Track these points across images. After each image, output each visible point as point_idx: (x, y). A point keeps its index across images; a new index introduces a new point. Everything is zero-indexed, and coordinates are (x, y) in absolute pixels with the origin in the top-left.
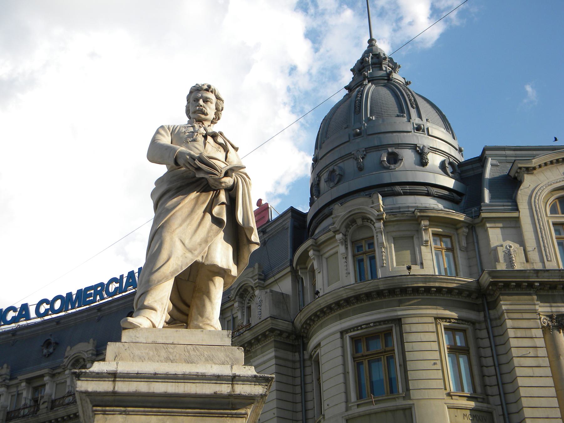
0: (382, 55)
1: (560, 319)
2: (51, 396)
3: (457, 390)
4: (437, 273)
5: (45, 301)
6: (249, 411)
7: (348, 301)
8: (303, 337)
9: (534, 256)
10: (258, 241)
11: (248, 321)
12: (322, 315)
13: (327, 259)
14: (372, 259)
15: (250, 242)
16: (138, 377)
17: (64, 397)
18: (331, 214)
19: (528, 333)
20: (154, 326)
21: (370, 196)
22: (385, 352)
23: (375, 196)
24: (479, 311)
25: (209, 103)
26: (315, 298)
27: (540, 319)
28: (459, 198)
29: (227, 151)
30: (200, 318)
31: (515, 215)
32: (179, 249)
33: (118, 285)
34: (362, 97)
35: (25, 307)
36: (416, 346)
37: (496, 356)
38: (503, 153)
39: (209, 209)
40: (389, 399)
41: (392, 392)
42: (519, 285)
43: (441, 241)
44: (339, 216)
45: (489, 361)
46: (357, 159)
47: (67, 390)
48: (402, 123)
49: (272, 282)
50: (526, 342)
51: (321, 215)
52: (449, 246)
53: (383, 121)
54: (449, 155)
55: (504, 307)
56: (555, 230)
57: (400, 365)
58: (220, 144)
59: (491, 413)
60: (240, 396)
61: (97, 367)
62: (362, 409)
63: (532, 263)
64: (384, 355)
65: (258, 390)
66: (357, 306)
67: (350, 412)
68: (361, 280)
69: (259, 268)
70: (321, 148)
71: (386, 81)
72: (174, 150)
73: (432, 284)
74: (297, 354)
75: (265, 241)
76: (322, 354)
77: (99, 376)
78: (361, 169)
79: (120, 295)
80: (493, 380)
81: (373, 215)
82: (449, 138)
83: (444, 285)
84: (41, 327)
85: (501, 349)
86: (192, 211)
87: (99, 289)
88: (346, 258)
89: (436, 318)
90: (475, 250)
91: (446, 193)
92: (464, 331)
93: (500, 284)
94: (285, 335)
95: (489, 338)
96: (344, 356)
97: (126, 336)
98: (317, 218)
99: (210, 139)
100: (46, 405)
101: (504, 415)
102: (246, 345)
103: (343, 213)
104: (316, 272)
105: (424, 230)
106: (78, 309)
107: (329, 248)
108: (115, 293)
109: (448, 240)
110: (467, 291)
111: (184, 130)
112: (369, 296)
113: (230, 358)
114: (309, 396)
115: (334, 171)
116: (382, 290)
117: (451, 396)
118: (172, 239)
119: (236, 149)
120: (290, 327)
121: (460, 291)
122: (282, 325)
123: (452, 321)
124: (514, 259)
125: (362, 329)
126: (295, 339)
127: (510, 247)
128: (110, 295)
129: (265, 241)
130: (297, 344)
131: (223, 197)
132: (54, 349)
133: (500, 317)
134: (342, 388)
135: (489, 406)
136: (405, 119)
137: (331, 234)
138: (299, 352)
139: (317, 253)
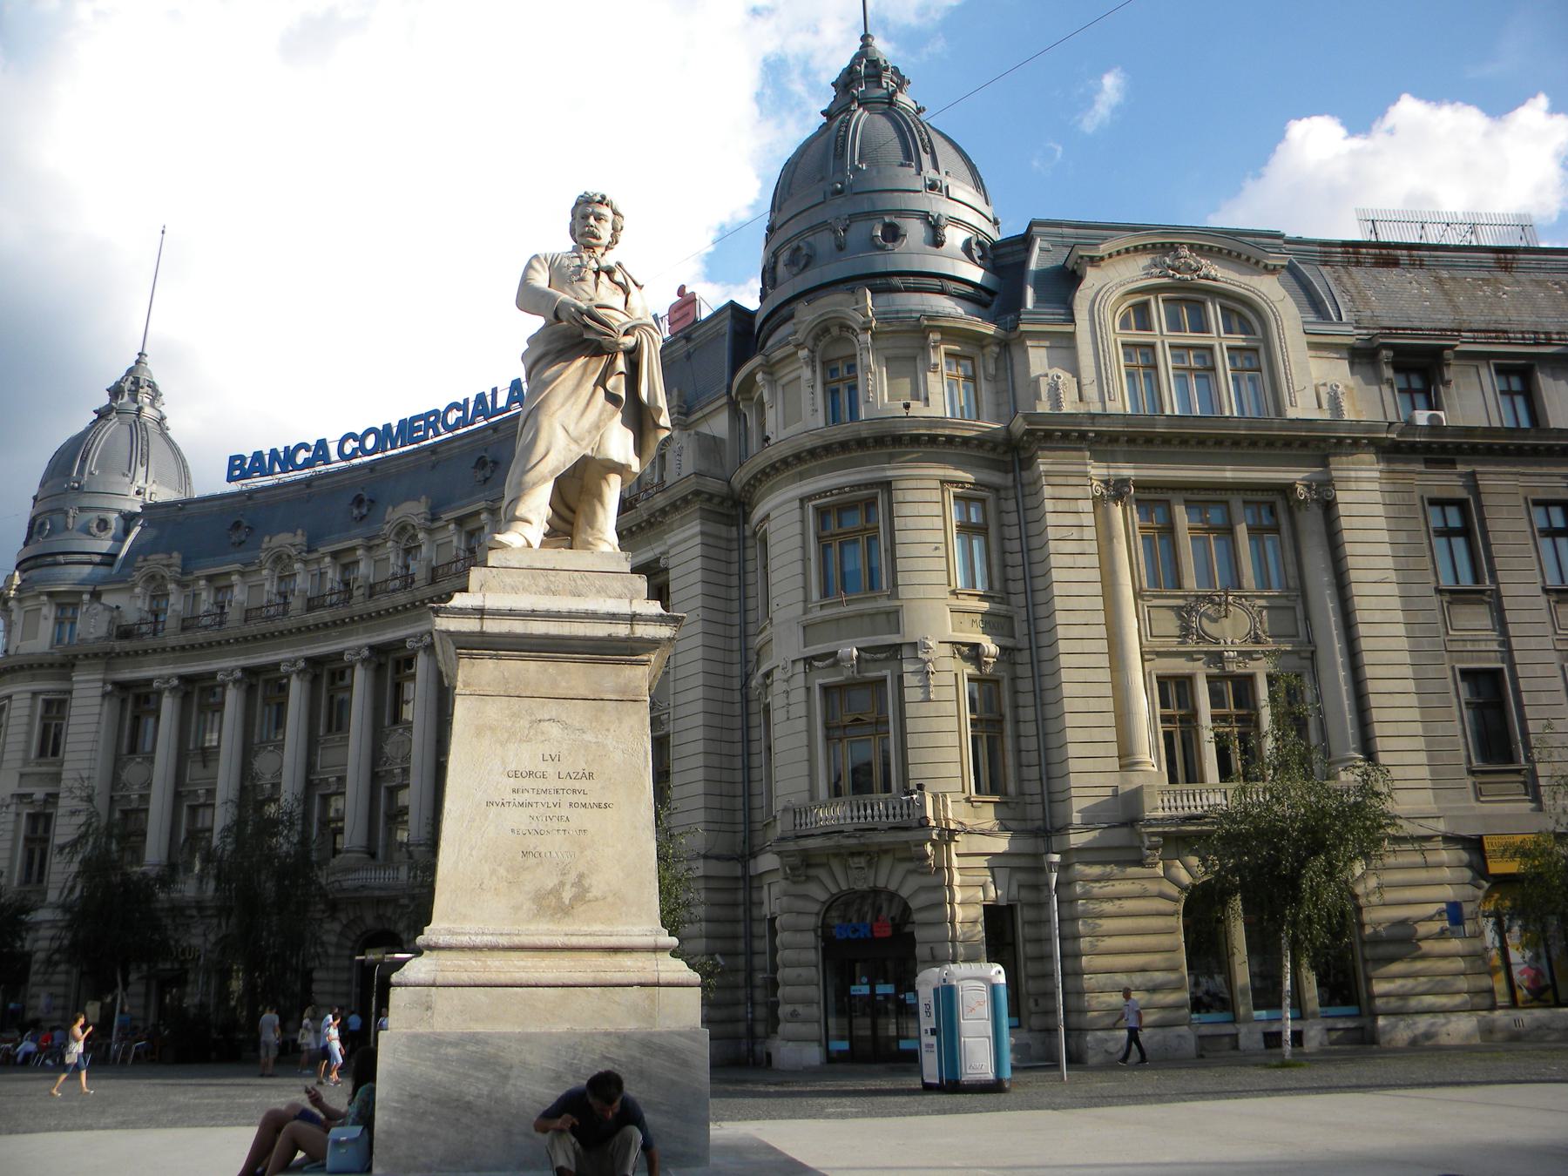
0: (882, 62)
1: (1119, 485)
2: (368, 578)
3: (967, 586)
4: (948, 415)
5: (351, 436)
6: (653, 658)
7: (813, 453)
8: (744, 504)
9: (1091, 392)
10: (669, 425)
11: (662, 476)
12: (773, 472)
13: (783, 386)
14: (853, 389)
15: (658, 427)
16: (511, 614)
17: (386, 581)
18: (791, 317)
19: (1072, 506)
20: (529, 545)
21: (853, 292)
22: (866, 529)
23: (860, 292)
24: (1006, 472)
25: (603, 222)
26: (764, 447)
27: (1091, 485)
28: (989, 298)
29: (627, 293)
30: (589, 530)
31: (1069, 329)
32: (560, 440)
33: (460, 414)
34: (847, 132)
35: (322, 444)
36: (911, 522)
37: (1025, 537)
38: (1059, 230)
39: (601, 382)
40: (867, 598)
41: (872, 588)
42: (1066, 435)
43: (958, 364)
44: (803, 322)
45: (1015, 545)
46: (835, 232)
47: (391, 571)
48: (908, 178)
49: (698, 419)
50: (1070, 519)
51: (777, 316)
52: (970, 373)
53: (879, 172)
54: (978, 231)
55: (1042, 468)
56: (1125, 354)
57: (886, 550)
58: (617, 284)
59: (1011, 618)
60: (641, 639)
61: (459, 600)
62: (827, 612)
63: (1088, 403)
64: (863, 535)
65: (664, 632)
66: (826, 460)
67: (809, 616)
68: (834, 422)
69: (680, 396)
70: (780, 210)
71: (887, 106)
72: (553, 298)
73: (940, 431)
74: (734, 529)
75: (689, 353)
76: (772, 529)
77: (462, 612)
78: (840, 248)
79: (465, 430)
80: (1018, 572)
81: (857, 321)
82: (979, 202)
83: (958, 433)
84: (347, 476)
85: (1033, 529)
86: (579, 385)
87: (432, 419)
88: (812, 386)
89: (942, 482)
90: (1006, 379)
91: (970, 290)
92: (983, 501)
93: (1039, 433)
94: (716, 500)
95: (1018, 511)
96: (804, 534)
97: (493, 558)
98: (770, 322)
99: (603, 276)
100: (361, 591)
101: (1028, 620)
102: (657, 514)
103: (810, 318)
104: (767, 406)
105: (933, 347)
106: (401, 450)
107: (787, 370)
108: (456, 427)
109: (968, 363)
110: (991, 442)
111: (567, 262)
112: (844, 446)
113: (629, 590)
114: (751, 591)
115: (798, 248)
116: (866, 438)
117: (957, 594)
118: (551, 426)
119: (639, 287)
120: (725, 489)
121: (980, 442)
122: (714, 485)
123: (966, 485)
124: (1062, 396)
125: (832, 495)
126: (732, 507)
127: (1059, 377)
128: (449, 429)
129: (689, 353)
130: (734, 513)
131: (621, 364)
132: (369, 510)
133: (1035, 484)
134: (799, 580)
135: (1009, 608)
136: (913, 171)
137: (790, 349)
138: (738, 526)
139: (769, 377)
